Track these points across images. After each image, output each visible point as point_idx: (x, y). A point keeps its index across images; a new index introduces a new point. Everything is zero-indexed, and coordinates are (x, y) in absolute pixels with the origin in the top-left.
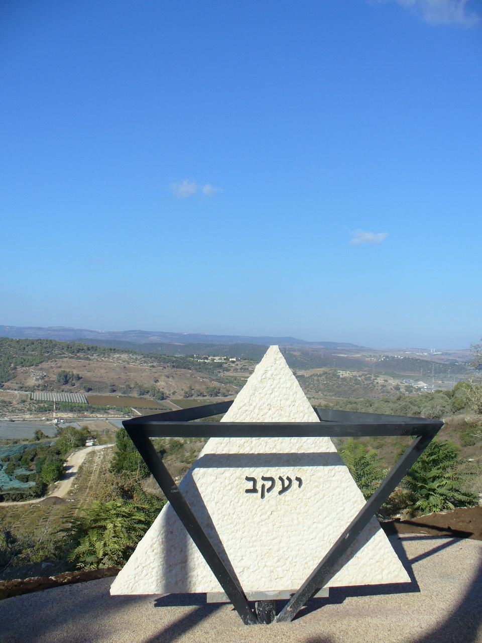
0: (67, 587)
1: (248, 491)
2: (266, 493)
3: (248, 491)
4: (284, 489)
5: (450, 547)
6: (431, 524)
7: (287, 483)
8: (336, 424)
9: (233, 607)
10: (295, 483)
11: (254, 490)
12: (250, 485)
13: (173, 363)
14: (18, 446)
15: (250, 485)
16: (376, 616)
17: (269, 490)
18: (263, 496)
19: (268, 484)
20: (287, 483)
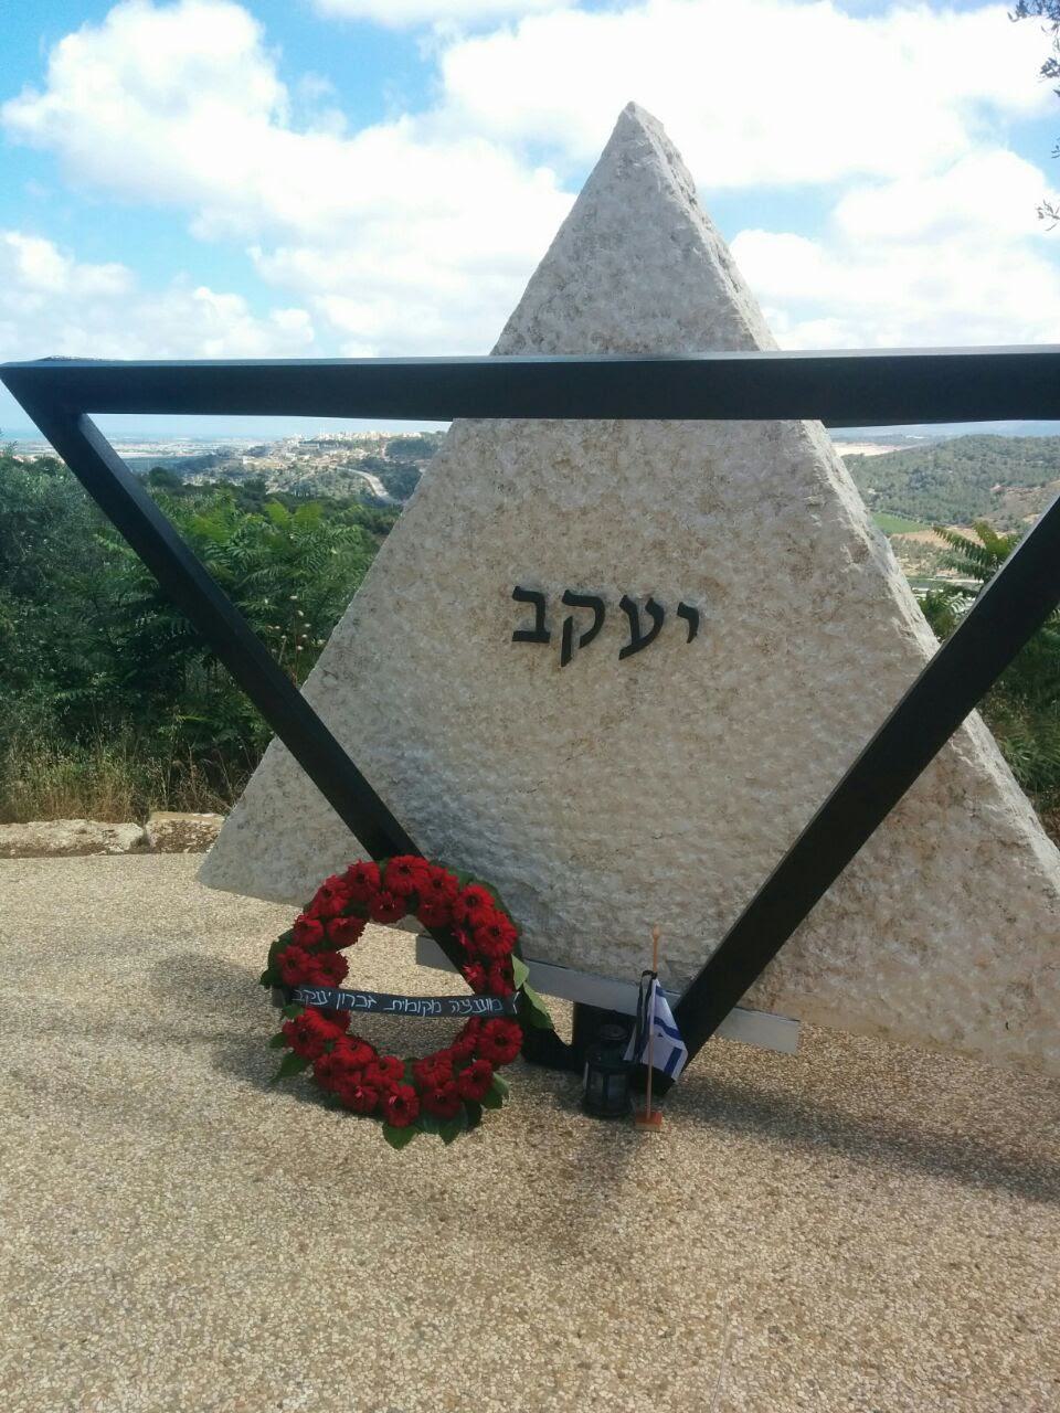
0: (119, 857)
1: (520, 636)
2: (575, 647)
3: (520, 636)
4: (638, 643)
5: (803, 815)
6: (815, 937)
7: (647, 622)
8: (37, 830)
9: (1029, 93)
10: (676, 626)
11: (538, 636)
12: (527, 617)
13: (760, 1351)
14: (686, 205)
15: (527, 617)
16: (523, 1098)
17: (587, 640)
18: (566, 658)
19: (586, 619)
20: (647, 622)
